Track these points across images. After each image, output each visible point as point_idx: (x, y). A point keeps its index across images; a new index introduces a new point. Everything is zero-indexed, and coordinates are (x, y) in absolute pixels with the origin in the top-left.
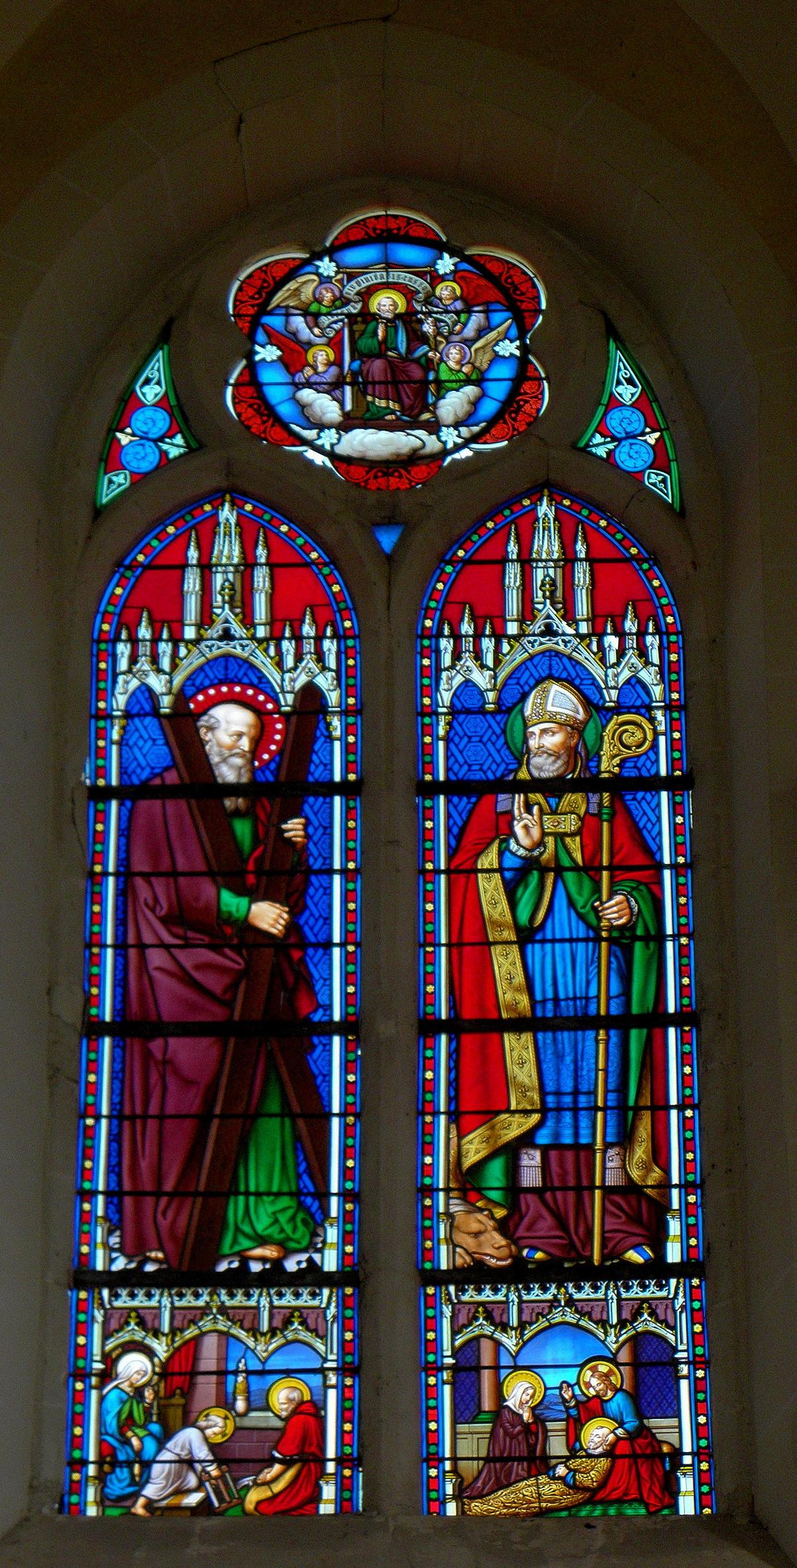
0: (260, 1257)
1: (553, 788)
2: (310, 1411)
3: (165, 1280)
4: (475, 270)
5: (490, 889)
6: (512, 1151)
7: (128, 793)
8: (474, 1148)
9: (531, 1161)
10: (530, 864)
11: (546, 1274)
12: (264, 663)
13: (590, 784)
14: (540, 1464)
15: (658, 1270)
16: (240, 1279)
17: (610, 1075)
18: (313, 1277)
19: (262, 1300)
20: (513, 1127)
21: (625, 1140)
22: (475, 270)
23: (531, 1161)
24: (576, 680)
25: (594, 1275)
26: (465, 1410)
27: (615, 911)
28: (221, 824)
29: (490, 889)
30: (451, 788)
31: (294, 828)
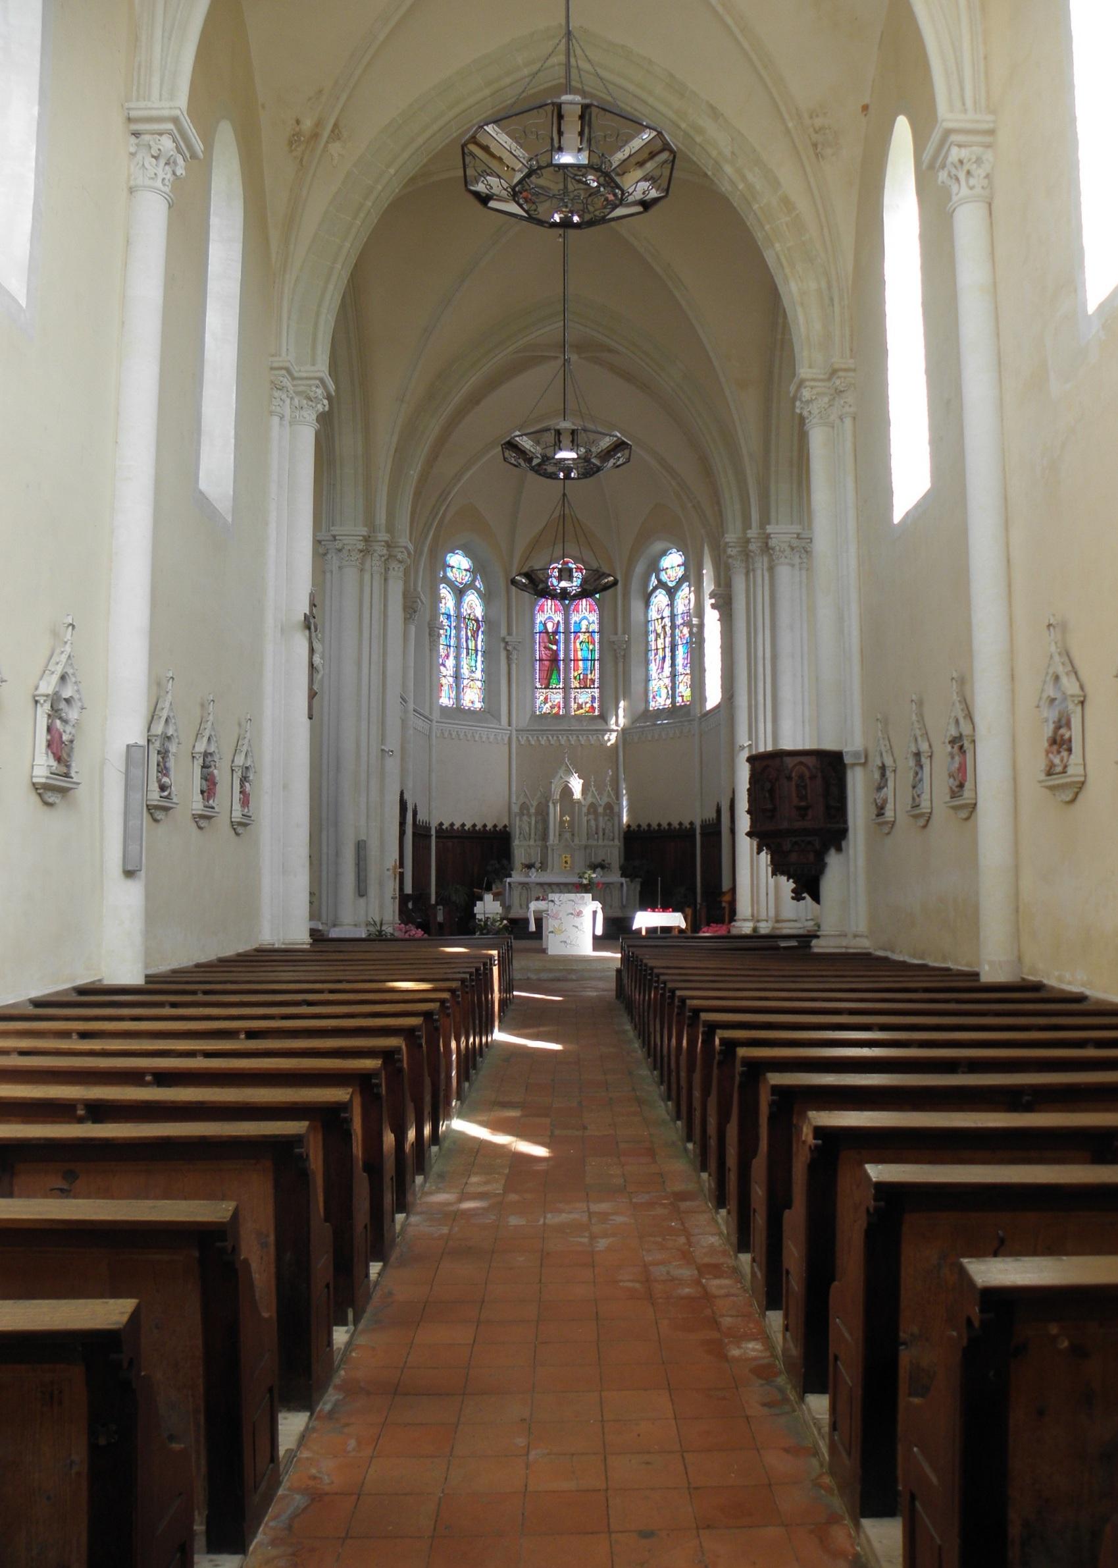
0: (554, 687)
1: (585, 633)
2: (559, 702)
3: (545, 688)
4: (671, 721)
5: (578, 644)
6: (580, 675)
7: (540, 633)
8: (576, 674)
9: (581, 676)
10: (582, 642)
11: (583, 688)
12: (553, 617)
13: (588, 632)
14: (582, 708)
15: (594, 688)
16: (552, 688)
17: (464, 637)
18: (559, 688)
19: (554, 691)
20: (580, 672)
21: (591, 673)
22: (671, 721)
23: (581, 676)
24: (587, 619)
25: (587, 688)
26: (575, 703)
27: (591, 647)
28: (549, 637)
29: (578, 644)
30: (574, 632)
31: (557, 637)
